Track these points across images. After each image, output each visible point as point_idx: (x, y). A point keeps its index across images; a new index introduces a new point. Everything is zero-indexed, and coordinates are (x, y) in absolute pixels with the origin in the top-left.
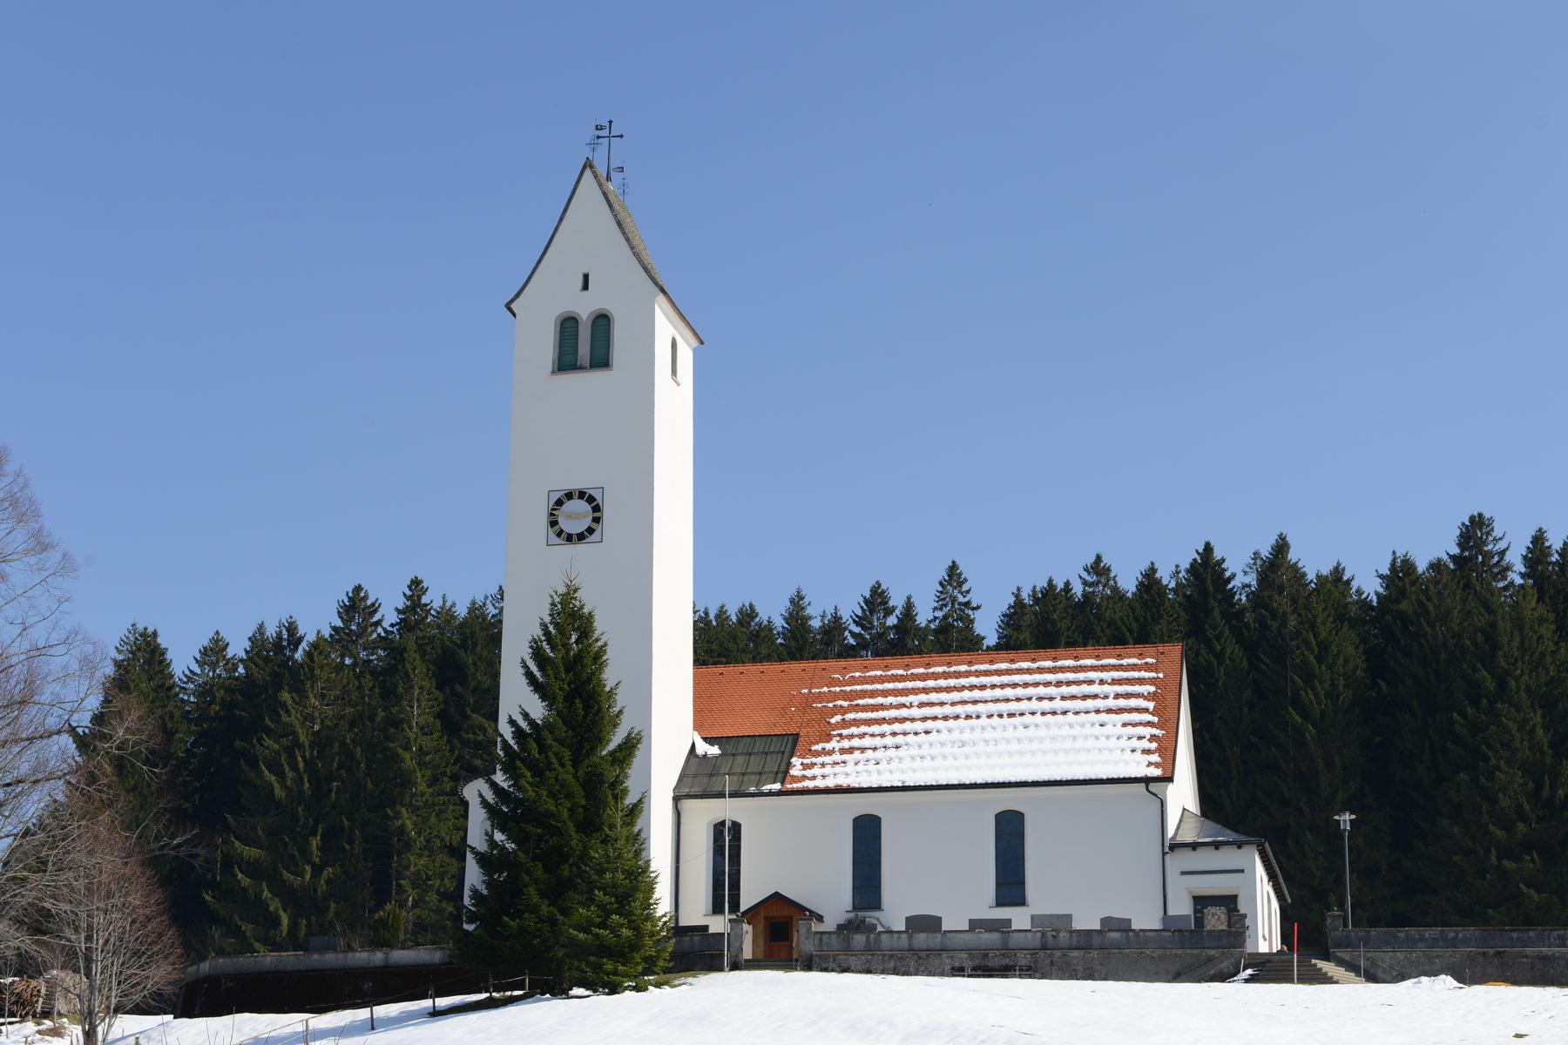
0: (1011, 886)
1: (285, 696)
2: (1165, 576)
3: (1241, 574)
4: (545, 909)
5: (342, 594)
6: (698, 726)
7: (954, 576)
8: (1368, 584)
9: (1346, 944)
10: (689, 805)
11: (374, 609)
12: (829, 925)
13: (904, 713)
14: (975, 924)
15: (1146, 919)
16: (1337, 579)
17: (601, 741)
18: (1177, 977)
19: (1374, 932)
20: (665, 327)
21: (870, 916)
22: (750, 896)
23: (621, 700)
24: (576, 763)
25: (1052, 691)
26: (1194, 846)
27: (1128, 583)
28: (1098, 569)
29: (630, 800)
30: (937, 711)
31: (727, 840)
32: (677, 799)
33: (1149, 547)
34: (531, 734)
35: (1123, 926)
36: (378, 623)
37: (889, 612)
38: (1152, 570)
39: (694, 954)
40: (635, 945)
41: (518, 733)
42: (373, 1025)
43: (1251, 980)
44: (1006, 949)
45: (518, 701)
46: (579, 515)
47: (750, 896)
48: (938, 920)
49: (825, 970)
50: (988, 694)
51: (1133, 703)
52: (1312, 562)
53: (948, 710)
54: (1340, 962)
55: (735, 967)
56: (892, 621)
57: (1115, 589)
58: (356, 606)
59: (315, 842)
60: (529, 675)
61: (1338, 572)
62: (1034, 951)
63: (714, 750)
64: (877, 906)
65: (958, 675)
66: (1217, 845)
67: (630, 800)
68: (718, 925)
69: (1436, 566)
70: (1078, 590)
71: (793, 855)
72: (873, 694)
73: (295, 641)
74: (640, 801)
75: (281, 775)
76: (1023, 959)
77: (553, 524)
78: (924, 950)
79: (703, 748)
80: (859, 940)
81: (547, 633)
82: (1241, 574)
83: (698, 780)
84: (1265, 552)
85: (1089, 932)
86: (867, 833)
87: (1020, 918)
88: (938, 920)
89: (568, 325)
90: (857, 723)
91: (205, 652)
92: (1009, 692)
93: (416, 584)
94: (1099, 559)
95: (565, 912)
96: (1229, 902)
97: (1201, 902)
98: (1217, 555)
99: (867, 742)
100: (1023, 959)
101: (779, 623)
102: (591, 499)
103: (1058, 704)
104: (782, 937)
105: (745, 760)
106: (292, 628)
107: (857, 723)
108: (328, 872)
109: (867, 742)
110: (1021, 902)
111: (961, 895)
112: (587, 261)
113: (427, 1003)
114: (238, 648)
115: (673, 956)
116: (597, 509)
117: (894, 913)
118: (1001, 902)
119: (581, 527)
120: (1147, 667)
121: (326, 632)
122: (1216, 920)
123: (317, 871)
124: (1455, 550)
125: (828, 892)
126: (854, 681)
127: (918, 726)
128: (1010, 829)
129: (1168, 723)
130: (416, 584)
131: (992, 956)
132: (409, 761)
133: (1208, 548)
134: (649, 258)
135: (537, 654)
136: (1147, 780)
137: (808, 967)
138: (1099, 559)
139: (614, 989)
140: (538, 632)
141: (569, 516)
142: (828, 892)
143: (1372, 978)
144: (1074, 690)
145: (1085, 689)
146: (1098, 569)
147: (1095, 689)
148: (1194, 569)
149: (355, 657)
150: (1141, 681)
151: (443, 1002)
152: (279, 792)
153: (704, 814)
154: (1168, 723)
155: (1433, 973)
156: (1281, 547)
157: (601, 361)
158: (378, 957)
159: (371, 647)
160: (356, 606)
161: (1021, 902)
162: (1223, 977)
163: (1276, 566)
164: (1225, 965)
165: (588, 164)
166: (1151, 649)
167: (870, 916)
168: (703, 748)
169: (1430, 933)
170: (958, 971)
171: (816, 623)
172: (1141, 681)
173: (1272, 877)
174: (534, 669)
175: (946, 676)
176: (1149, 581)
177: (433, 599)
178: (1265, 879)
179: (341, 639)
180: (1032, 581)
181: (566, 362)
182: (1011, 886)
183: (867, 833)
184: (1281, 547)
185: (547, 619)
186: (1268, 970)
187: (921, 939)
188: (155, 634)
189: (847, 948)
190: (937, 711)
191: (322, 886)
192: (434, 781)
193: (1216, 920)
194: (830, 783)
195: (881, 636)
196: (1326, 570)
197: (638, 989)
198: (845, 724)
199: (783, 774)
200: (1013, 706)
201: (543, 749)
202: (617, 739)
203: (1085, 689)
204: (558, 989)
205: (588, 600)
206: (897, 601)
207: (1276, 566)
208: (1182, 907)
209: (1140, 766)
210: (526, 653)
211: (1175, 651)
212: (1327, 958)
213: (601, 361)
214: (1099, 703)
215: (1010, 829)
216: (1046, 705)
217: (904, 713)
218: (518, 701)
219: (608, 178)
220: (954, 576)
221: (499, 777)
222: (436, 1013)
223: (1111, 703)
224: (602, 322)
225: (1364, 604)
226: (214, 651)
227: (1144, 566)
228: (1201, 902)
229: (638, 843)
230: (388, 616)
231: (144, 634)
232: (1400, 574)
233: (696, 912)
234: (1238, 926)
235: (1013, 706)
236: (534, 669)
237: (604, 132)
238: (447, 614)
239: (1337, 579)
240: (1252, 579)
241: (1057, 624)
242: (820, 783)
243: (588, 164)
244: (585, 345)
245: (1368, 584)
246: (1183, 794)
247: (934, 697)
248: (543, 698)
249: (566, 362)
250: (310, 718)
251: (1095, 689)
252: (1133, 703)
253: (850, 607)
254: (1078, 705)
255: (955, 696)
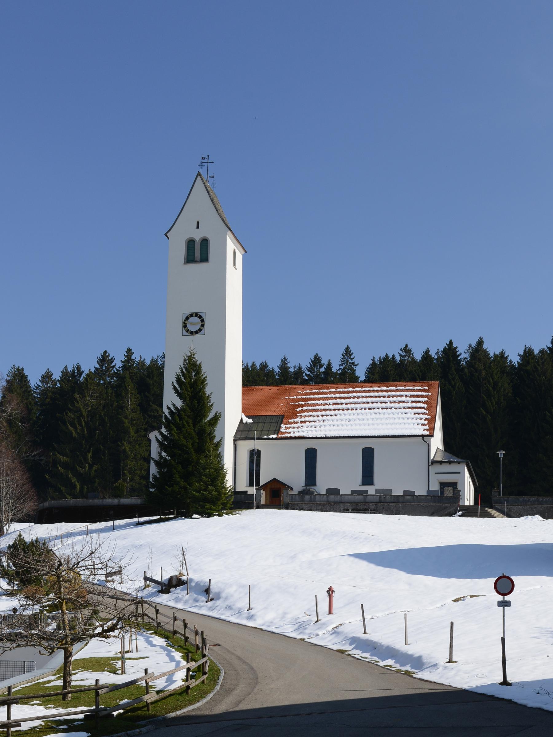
0: (368, 476)
1: (76, 396)
2: (433, 353)
3: (464, 354)
4: (182, 484)
5: (98, 354)
6: (244, 411)
7: (348, 352)
8: (514, 358)
9: (500, 502)
10: (240, 443)
11: (112, 361)
12: (295, 492)
13: (326, 407)
14: (353, 492)
15: (421, 491)
16: (502, 357)
17: (205, 416)
18: (432, 514)
19: (511, 498)
20: (231, 245)
21: (312, 488)
22: (263, 480)
23: (213, 400)
24: (194, 425)
25: (386, 399)
26: (441, 463)
27: (418, 356)
28: (406, 350)
29: (216, 440)
30: (340, 406)
31: (255, 457)
32: (235, 440)
33: (427, 343)
34: (176, 413)
35: (412, 494)
36: (114, 366)
37: (321, 366)
38: (428, 351)
39: (241, 502)
40: (218, 498)
41: (171, 412)
42: (114, 528)
43: (460, 516)
44: (365, 502)
45: (171, 399)
46: (196, 323)
47: (263, 480)
48: (338, 490)
49: (294, 509)
50: (360, 400)
51: (419, 405)
52: (492, 349)
53: (344, 406)
54: (497, 510)
55: (258, 507)
56: (322, 370)
57: (413, 358)
58: (105, 359)
59: (89, 455)
60: (175, 389)
61: (502, 353)
62: (376, 503)
63: (250, 421)
64: (315, 484)
65: (348, 392)
66: (450, 463)
67: (216, 440)
68: (251, 491)
69: (542, 352)
70: (398, 358)
71: (281, 463)
72: (314, 399)
73: (80, 373)
74: (220, 441)
75: (75, 428)
76: (372, 506)
77: (185, 327)
78: (333, 502)
79: (245, 420)
80: (307, 497)
81: (182, 372)
82: (464, 354)
83: (244, 433)
84: (474, 345)
85: (398, 496)
86: (311, 455)
87: (371, 490)
88: (338, 490)
89: (191, 243)
90: (307, 411)
91: (43, 377)
92: (369, 400)
93: (129, 350)
94: (407, 346)
95: (190, 485)
96: (454, 485)
97: (443, 485)
98: (455, 345)
99: (312, 419)
100: (372, 506)
101: (277, 370)
102: (200, 317)
103: (388, 405)
104: (276, 496)
105: (262, 425)
106: (79, 368)
107: (307, 411)
108: (95, 467)
109: (312, 419)
110: (372, 483)
111: (349, 482)
112: (198, 216)
113: (135, 520)
114: (57, 376)
115: (233, 503)
116: (203, 321)
117: (322, 486)
118: (364, 483)
119: (191, 319)
120: (425, 391)
121: (93, 370)
122: (448, 492)
123: (91, 467)
124: (550, 346)
125: (295, 478)
126: (307, 394)
127: (332, 412)
128: (368, 455)
129: (432, 413)
130: (129, 350)
131: (359, 505)
132: (127, 423)
133: (451, 342)
134: (224, 216)
135: (179, 380)
136: (423, 436)
137: (287, 508)
138: (407, 346)
139: (210, 515)
140: (179, 371)
141: (191, 324)
142: (295, 478)
143: (509, 516)
144: (395, 399)
145: (400, 399)
146: (406, 350)
147: (404, 399)
148: (445, 351)
149: (104, 380)
150: (422, 396)
151: (142, 519)
152: (75, 435)
153: (246, 446)
154: (432, 413)
155: (533, 514)
156: (480, 342)
157: (205, 259)
158: (116, 501)
159: (111, 376)
160: (105, 359)
161: (372, 483)
162: (450, 514)
163: (478, 350)
164: (451, 510)
165: (199, 174)
166: (427, 383)
167: (312, 488)
168: (245, 420)
169: (532, 498)
170: (346, 511)
171: (292, 370)
172: (422, 396)
173: (471, 475)
174: (177, 386)
175: (344, 392)
176: (427, 355)
177: (136, 357)
178: (469, 476)
179: (99, 373)
180: (379, 354)
181: (190, 259)
182: (368, 476)
183: (311, 455)
184: (480, 342)
185: (183, 366)
186: (468, 512)
187: (332, 498)
188: (23, 369)
189: (303, 501)
190: (340, 406)
191: (93, 473)
192: (137, 431)
193: (448, 492)
194: (297, 435)
195: (318, 376)
196: (498, 352)
197: (219, 515)
198: (303, 411)
199: (278, 431)
200: (370, 405)
201: (181, 419)
202: (211, 416)
203: (400, 399)
204: (188, 516)
205: (199, 358)
206: (325, 362)
207: (478, 350)
208: (435, 487)
209: (420, 430)
210: (174, 380)
211: (436, 384)
212: (491, 508)
213: (205, 259)
214: (405, 405)
215: (368, 455)
216: (384, 405)
217: (326, 407)
218: (171, 399)
219: (207, 181)
220: (348, 352)
221: (164, 430)
222: (139, 524)
223: (410, 405)
224: (205, 242)
225: (513, 367)
226: (47, 377)
227: (425, 349)
228: (443, 485)
229: (219, 458)
230: (118, 364)
231: (18, 369)
232: (528, 354)
233: (243, 485)
234: (457, 494)
235: (370, 405)
236: (177, 386)
237: (205, 160)
238: (142, 363)
239: (502, 357)
240: (468, 356)
241: (389, 372)
242: (292, 435)
243: (199, 174)
244: (198, 252)
245: (514, 358)
246: (437, 442)
247: (339, 401)
248: (181, 398)
249: (190, 259)
250: (87, 405)
251: (404, 399)
252: (419, 405)
253: (305, 364)
254: (397, 405)
255: (347, 401)
